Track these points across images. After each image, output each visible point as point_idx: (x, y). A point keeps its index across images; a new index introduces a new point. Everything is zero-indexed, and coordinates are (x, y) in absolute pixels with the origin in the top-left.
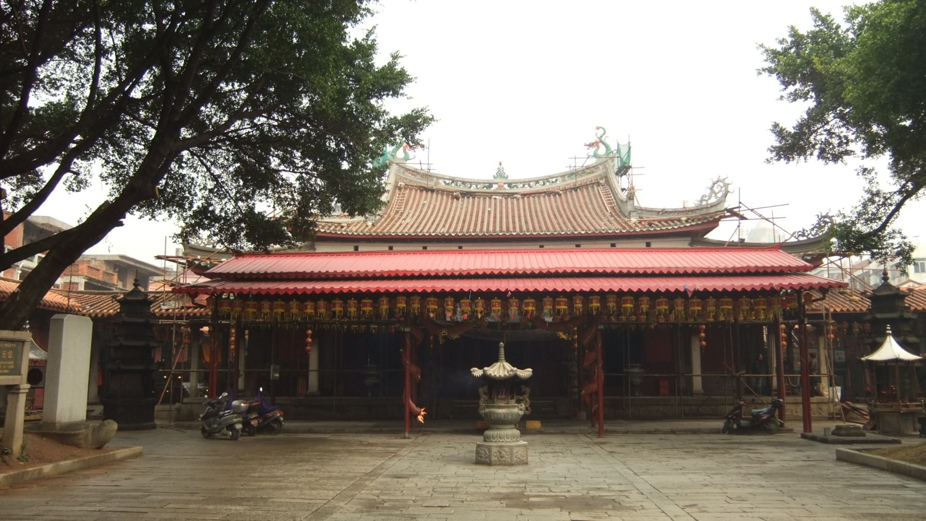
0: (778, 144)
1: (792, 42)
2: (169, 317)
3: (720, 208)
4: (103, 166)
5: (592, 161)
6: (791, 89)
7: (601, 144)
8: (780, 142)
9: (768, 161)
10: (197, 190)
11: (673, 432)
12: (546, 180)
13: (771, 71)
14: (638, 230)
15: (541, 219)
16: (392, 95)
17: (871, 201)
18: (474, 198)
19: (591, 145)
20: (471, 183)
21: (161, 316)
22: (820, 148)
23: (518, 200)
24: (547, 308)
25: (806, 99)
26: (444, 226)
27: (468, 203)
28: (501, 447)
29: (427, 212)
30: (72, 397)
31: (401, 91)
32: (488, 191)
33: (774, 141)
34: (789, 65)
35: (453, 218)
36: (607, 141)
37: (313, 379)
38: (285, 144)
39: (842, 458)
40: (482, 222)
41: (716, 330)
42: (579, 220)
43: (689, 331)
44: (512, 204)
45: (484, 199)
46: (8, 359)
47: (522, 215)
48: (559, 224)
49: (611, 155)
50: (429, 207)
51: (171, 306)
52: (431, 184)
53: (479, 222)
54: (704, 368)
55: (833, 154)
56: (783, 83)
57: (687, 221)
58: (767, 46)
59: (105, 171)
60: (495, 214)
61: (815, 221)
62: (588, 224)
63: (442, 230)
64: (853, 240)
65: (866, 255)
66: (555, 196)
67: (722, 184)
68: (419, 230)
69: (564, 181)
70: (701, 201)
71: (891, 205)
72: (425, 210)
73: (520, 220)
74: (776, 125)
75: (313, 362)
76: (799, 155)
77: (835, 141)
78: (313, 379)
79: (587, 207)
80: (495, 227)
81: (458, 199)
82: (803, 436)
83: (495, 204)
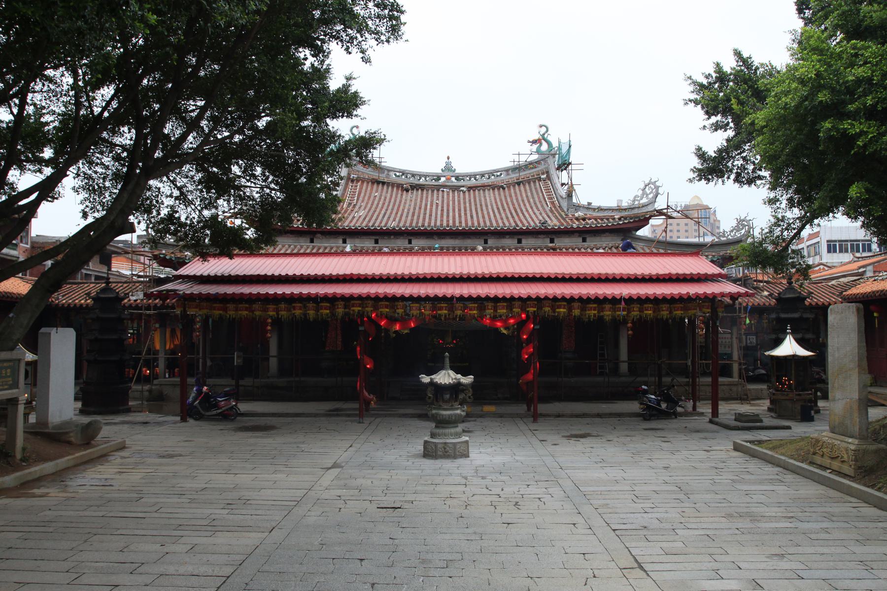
0: (700, 167)
1: (716, 77)
2: (137, 307)
3: (650, 208)
4: (74, 178)
5: (535, 157)
6: (714, 119)
8: (702, 165)
9: (691, 181)
10: (164, 199)
11: (599, 416)
12: (491, 173)
13: (696, 102)
14: (575, 226)
15: (485, 213)
16: (347, 117)
17: (776, 224)
18: (422, 190)
19: (534, 142)
20: (421, 176)
22: (737, 173)
23: (464, 192)
24: (489, 312)
25: (726, 130)
26: (394, 220)
27: (417, 196)
28: (445, 443)
29: (378, 204)
30: (62, 401)
31: (355, 113)
32: (436, 183)
33: (696, 163)
34: (712, 101)
35: (403, 210)
36: (549, 138)
37: (273, 363)
38: (244, 151)
39: (737, 448)
40: (431, 215)
41: (641, 325)
42: (521, 215)
43: (617, 324)
44: (459, 197)
45: (433, 191)
46: (7, 377)
47: (468, 209)
48: (502, 219)
49: (553, 152)
50: (380, 199)
51: (137, 296)
52: (383, 177)
53: (427, 216)
54: (630, 352)
55: (745, 179)
56: (707, 113)
57: (620, 219)
59: (78, 183)
60: (442, 207)
61: (734, 223)
62: (529, 219)
66: (499, 189)
67: (653, 186)
68: (370, 224)
69: (508, 174)
70: (634, 201)
71: (794, 229)
72: (376, 202)
73: (466, 214)
74: (699, 149)
75: (273, 350)
76: (718, 177)
77: (751, 167)
78: (273, 363)
79: (529, 202)
80: (442, 221)
81: (407, 191)
82: (711, 422)
83: (443, 197)
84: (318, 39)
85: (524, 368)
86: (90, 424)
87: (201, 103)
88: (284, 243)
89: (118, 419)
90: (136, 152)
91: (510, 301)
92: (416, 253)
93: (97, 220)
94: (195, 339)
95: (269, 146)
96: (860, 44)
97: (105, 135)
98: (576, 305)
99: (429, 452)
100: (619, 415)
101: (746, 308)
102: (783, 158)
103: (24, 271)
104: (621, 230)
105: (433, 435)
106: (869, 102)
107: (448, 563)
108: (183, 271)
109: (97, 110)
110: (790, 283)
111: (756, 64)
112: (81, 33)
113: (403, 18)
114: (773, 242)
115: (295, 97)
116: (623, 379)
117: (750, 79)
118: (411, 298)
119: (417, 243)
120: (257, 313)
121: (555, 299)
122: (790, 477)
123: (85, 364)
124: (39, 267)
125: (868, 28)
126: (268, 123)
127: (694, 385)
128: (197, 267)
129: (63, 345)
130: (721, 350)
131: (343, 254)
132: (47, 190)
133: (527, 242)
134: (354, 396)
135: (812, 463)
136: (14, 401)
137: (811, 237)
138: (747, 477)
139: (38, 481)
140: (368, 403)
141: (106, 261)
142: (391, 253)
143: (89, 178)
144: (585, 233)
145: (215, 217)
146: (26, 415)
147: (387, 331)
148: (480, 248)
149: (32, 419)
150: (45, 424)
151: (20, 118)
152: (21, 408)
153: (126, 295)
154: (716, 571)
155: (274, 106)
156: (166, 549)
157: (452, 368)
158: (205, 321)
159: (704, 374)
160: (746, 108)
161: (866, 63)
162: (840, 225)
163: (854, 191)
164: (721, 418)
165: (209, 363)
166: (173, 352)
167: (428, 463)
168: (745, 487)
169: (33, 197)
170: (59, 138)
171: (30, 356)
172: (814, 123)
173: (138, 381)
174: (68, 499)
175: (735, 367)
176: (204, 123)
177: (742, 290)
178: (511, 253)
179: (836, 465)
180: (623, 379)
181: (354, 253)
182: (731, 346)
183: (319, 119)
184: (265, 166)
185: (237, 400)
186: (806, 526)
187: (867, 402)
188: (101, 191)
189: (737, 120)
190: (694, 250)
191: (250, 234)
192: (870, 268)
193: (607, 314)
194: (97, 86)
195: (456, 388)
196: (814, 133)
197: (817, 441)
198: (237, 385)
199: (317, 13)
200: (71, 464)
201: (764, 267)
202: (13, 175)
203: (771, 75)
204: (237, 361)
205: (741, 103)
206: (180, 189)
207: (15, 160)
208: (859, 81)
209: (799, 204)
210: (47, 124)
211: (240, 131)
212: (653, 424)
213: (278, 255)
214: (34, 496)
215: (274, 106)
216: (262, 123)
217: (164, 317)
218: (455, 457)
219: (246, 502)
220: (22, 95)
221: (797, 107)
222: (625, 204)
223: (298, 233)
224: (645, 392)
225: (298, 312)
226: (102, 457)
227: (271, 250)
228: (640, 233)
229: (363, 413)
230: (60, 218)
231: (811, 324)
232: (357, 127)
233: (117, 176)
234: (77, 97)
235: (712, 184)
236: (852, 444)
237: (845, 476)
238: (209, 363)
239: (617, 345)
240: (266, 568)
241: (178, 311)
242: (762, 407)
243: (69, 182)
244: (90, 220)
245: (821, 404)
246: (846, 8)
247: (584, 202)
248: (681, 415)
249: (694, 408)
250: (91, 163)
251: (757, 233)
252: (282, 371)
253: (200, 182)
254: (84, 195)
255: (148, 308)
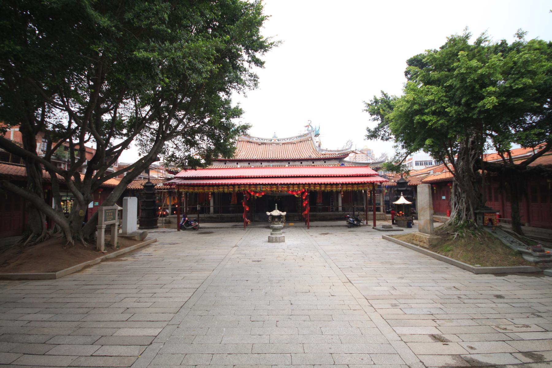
2: (160, 189)
3: (349, 150)
5: (307, 132)
6: (373, 117)
11: (332, 226)
12: (290, 138)
13: (367, 111)
17: (397, 155)
19: (306, 126)
21: (158, 189)
24: (291, 189)
30: (132, 224)
33: (367, 133)
36: (312, 125)
37: (212, 209)
39: (384, 238)
41: (346, 193)
43: (338, 193)
51: (160, 185)
52: (251, 140)
58: (366, 102)
63: (255, 158)
64: (391, 167)
65: (395, 172)
75: (212, 204)
77: (387, 134)
78: (212, 209)
82: (373, 228)
84: (227, 88)
85: (304, 209)
86: (143, 233)
87: (184, 113)
88: (215, 165)
89: (153, 231)
90: (159, 131)
91: (299, 185)
92: (264, 168)
93: (145, 157)
94: (182, 201)
95: (209, 129)
96: (430, 87)
97: (147, 124)
98: (323, 186)
99: (270, 240)
100: (339, 226)
101: (385, 186)
102: (400, 130)
103: (115, 176)
104: (339, 159)
105: (272, 234)
106: (433, 109)
107: (279, 281)
108: (178, 175)
109: (144, 115)
110: (402, 177)
111: (389, 96)
112: (140, 85)
113: (259, 80)
114: (395, 162)
115: (219, 110)
116: (340, 213)
117: (387, 101)
118: (263, 184)
119: (264, 164)
120: (206, 190)
121: (315, 184)
122: (404, 248)
123: (140, 210)
124: (122, 175)
125: (433, 81)
126: (209, 121)
127: (367, 215)
128: (183, 174)
129: (132, 203)
130: (377, 202)
131: (237, 168)
132: (125, 145)
133: (304, 163)
134: (242, 220)
135: (412, 243)
136: (114, 225)
137: (409, 160)
138: (388, 248)
139: (123, 255)
140: (247, 223)
141: (148, 172)
142: (255, 168)
143: (141, 141)
144: (325, 160)
145: (189, 155)
146: (118, 230)
147: (254, 196)
148: (287, 166)
149: (121, 231)
150: (126, 233)
151: (114, 118)
152: (116, 227)
153: (156, 185)
154: (379, 283)
155: (211, 114)
156: (173, 279)
157: (278, 209)
158: (186, 194)
159: (370, 211)
160: (386, 112)
161: (432, 94)
162: (422, 155)
163: (428, 142)
164: (377, 227)
165: (188, 209)
166: (174, 205)
167: (270, 244)
168: (387, 252)
169: (120, 148)
170: (129, 126)
171: (120, 208)
172: (412, 117)
173: (161, 216)
174: (135, 261)
175: (382, 208)
176: (185, 120)
177: (384, 180)
178: (298, 167)
179: (421, 244)
180: (340, 213)
181: (241, 168)
182: (380, 200)
183: (227, 119)
184: (208, 136)
185: (199, 223)
186: (411, 266)
187: (433, 221)
188: (146, 145)
189: (382, 117)
190: (367, 165)
191: (203, 161)
192: (432, 171)
193: (334, 189)
194: (143, 106)
195: (280, 217)
196: (412, 121)
197: (414, 235)
198: (198, 217)
199: (227, 79)
200: (136, 248)
201: (392, 171)
202: (112, 140)
203: (395, 100)
204: (198, 208)
205: (384, 110)
206: (176, 145)
207: (112, 135)
208: (429, 101)
209: (406, 147)
210: (124, 120)
211: (198, 123)
212: (352, 229)
213: (213, 169)
214: (122, 260)
215: (211, 114)
216: (206, 120)
217: (170, 193)
218: (280, 242)
219: (204, 260)
220: (116, 107)
221: (406, 111)
222: (340, 149)
223: (221, 161)
224: (349, 217)
225: (221, 190)
226: (148, 245)
227: (210, 167)
228: (345, 159)
229: (246, 226)
230: (130, 156)
231: (411, 192)
233: (152, 140)
234: (136, 110)
235: (372, 141)
236: (428, 236)
237: (425, 248)
238: (188, 209)
239: (337, 201)
240: (212, 284)
241: (176, 190)
242: (389, 223)
243: (133, 143)
244: (142, 156)
245: (414, 221)
246: (424, 73)
247: (325, 149)
248: (362, 226)
249: (367, 223)
250: (141, 135)
251: (389, 159)
252: (215, 212)
253: (184, 142)
254: (139, 147)
255: (164, 189)
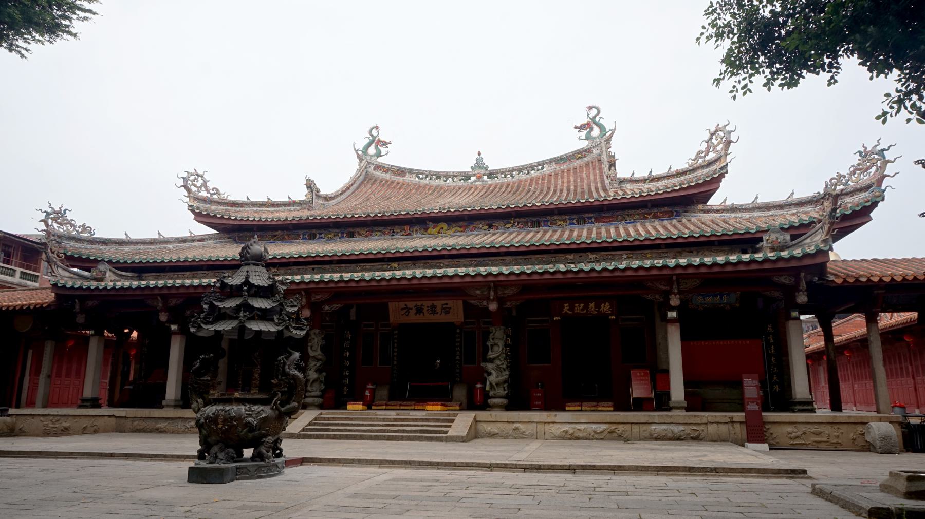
5: (585, 144)
7: (594, 126)
9: (832, 81)
19: (581, 128)
36: (602, 121)
61: (856, 160)
70: (696, 159)
232: (377, 128)
